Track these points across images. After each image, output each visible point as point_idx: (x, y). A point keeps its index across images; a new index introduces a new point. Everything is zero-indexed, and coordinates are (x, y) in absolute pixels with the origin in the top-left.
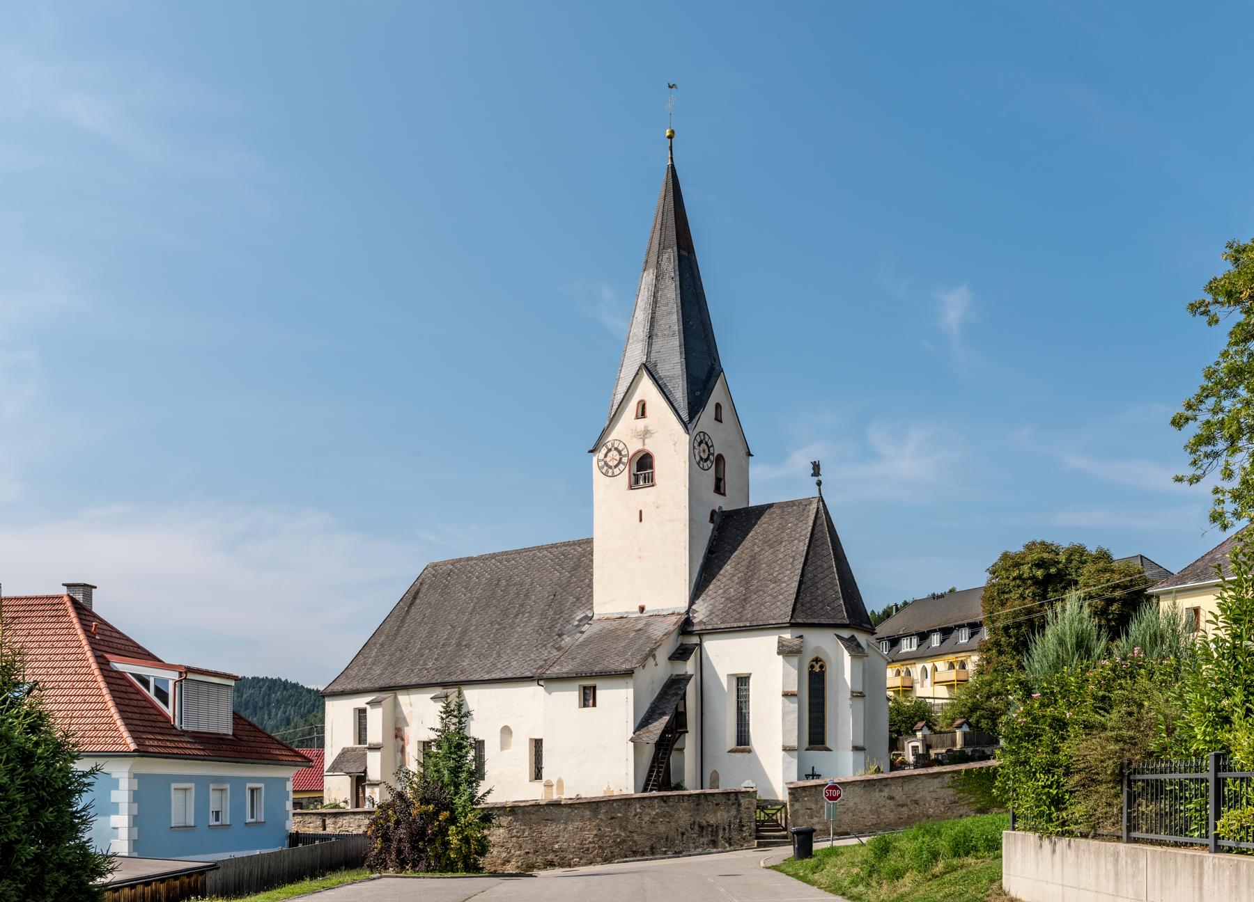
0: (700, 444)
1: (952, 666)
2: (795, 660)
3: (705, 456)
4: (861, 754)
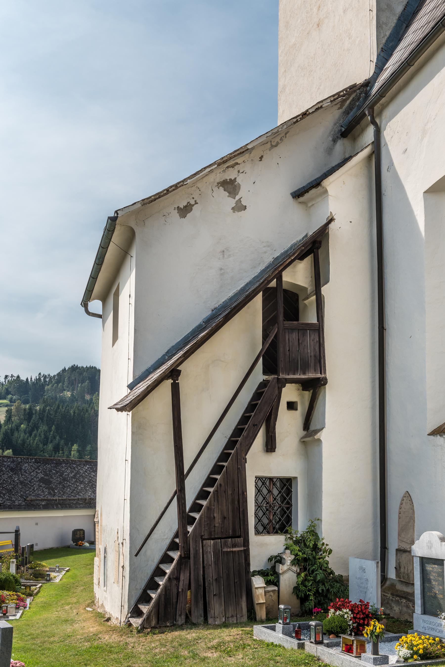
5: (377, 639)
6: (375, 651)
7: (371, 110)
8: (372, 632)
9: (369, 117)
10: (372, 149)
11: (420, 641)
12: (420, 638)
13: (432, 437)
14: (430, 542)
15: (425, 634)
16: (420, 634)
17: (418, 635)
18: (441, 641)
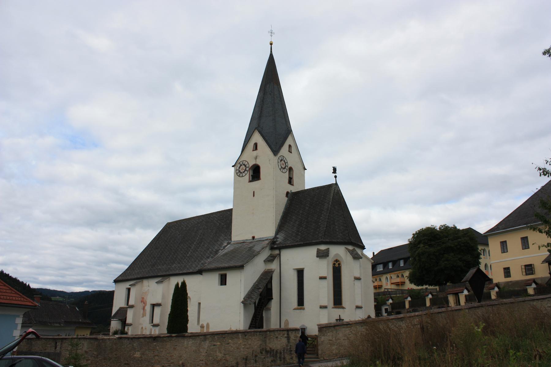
0: (281, 160)
1: (398, 276)
3: (284, 167)
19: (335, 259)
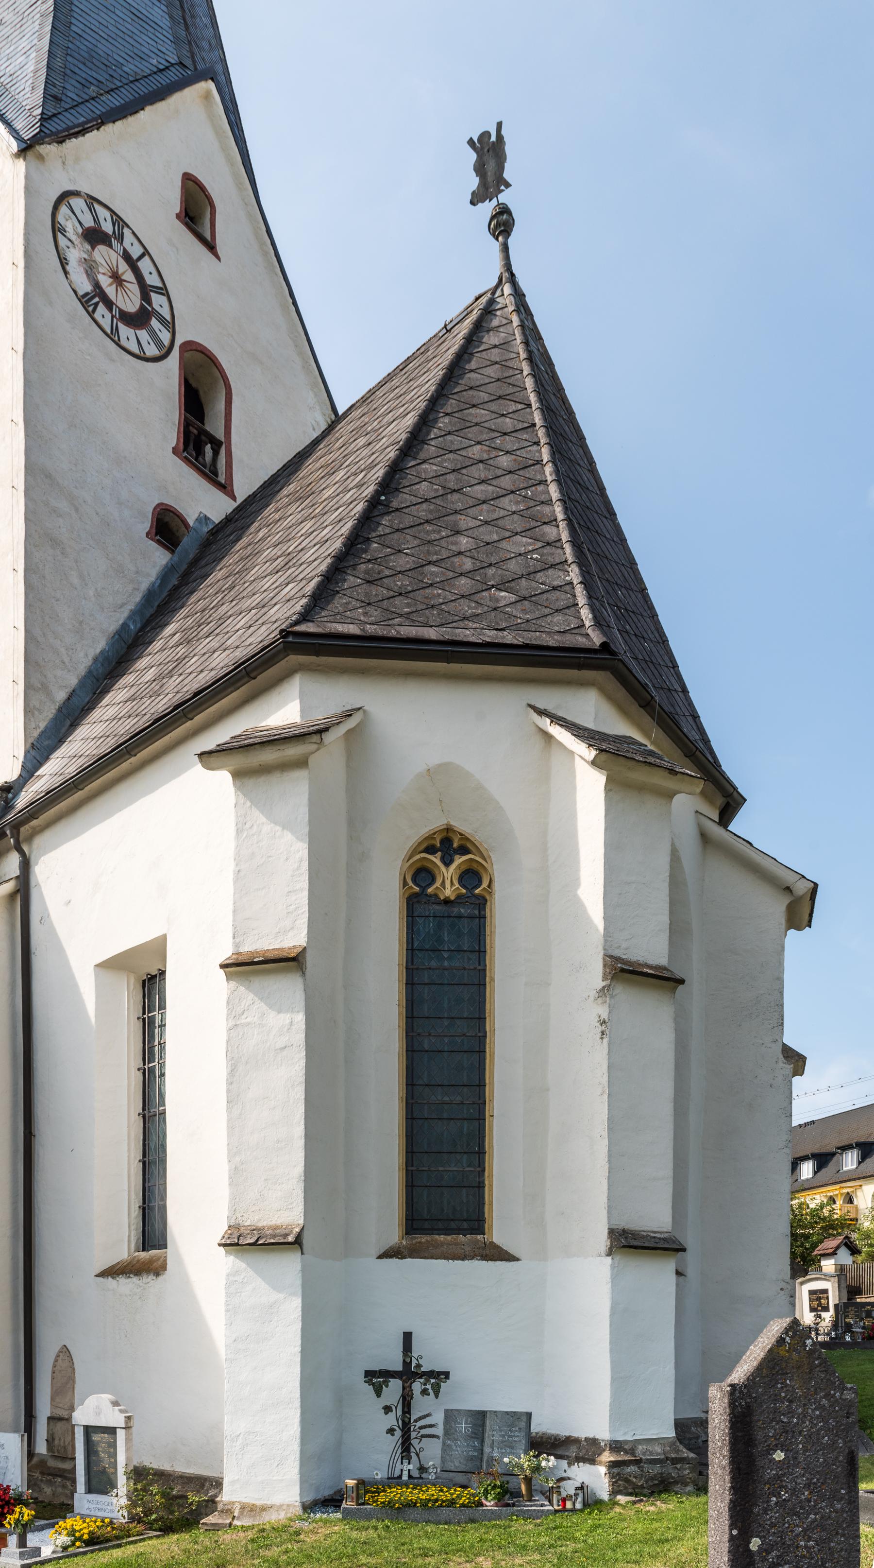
2: (295, 793)
4: (658, 1277)
5: (24, 1529)
6: (22, 1543)
7: (15, 831)
8: (17, 1521)
9: (12, 840)
10: (16, 886)
11: (85, 1525)
12: (84, 1522)
13: (101, 1279)
14: (98, 1407)
15: (89, 1516)
16: (83, 1517)
17: (82, 1518)
18: (111, 1522)
19: (431, 823)
